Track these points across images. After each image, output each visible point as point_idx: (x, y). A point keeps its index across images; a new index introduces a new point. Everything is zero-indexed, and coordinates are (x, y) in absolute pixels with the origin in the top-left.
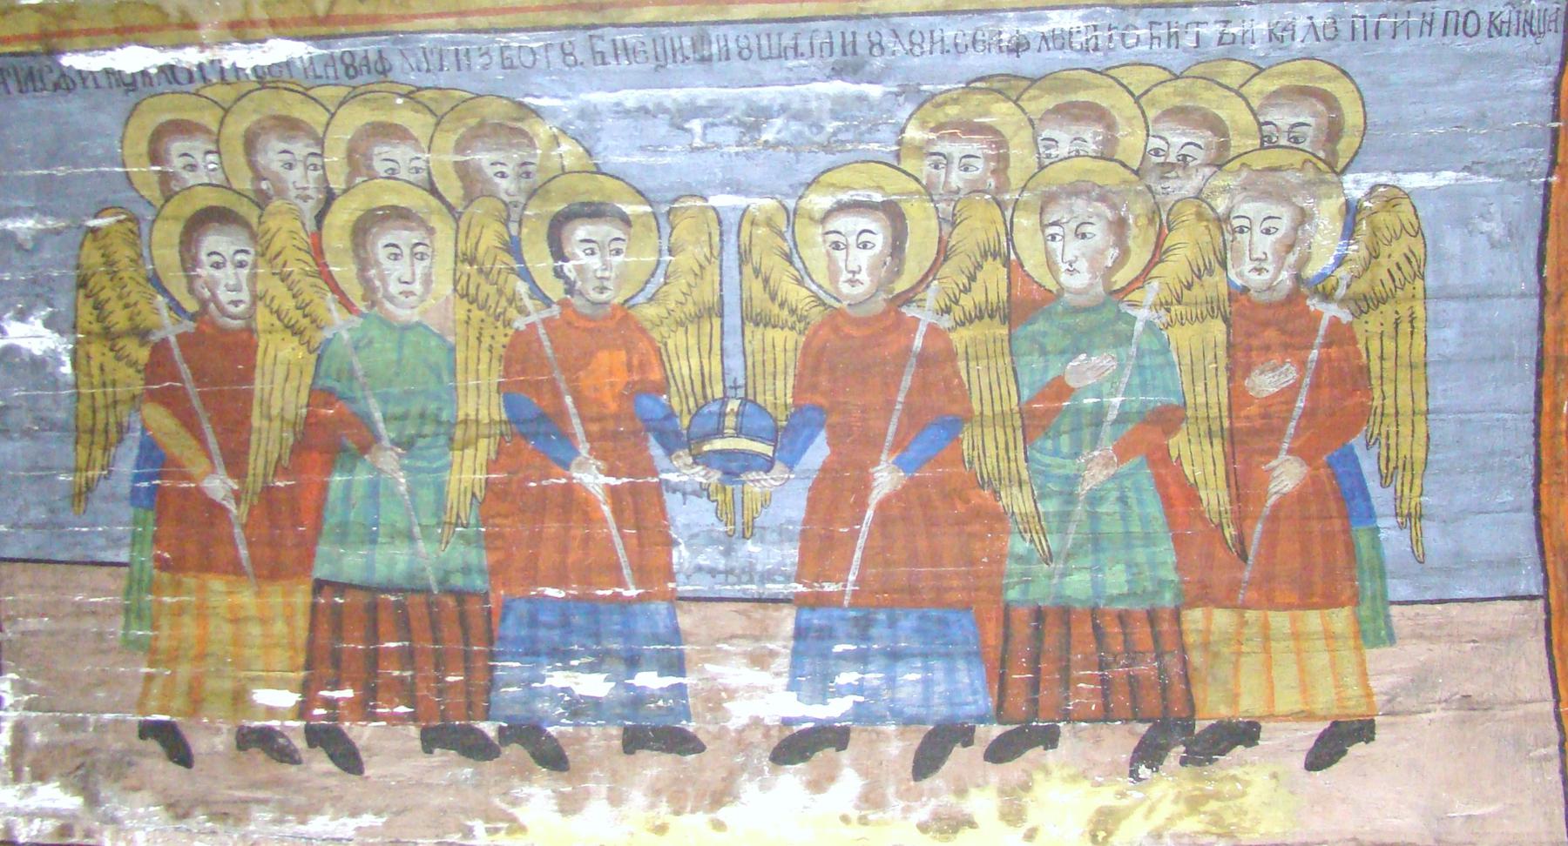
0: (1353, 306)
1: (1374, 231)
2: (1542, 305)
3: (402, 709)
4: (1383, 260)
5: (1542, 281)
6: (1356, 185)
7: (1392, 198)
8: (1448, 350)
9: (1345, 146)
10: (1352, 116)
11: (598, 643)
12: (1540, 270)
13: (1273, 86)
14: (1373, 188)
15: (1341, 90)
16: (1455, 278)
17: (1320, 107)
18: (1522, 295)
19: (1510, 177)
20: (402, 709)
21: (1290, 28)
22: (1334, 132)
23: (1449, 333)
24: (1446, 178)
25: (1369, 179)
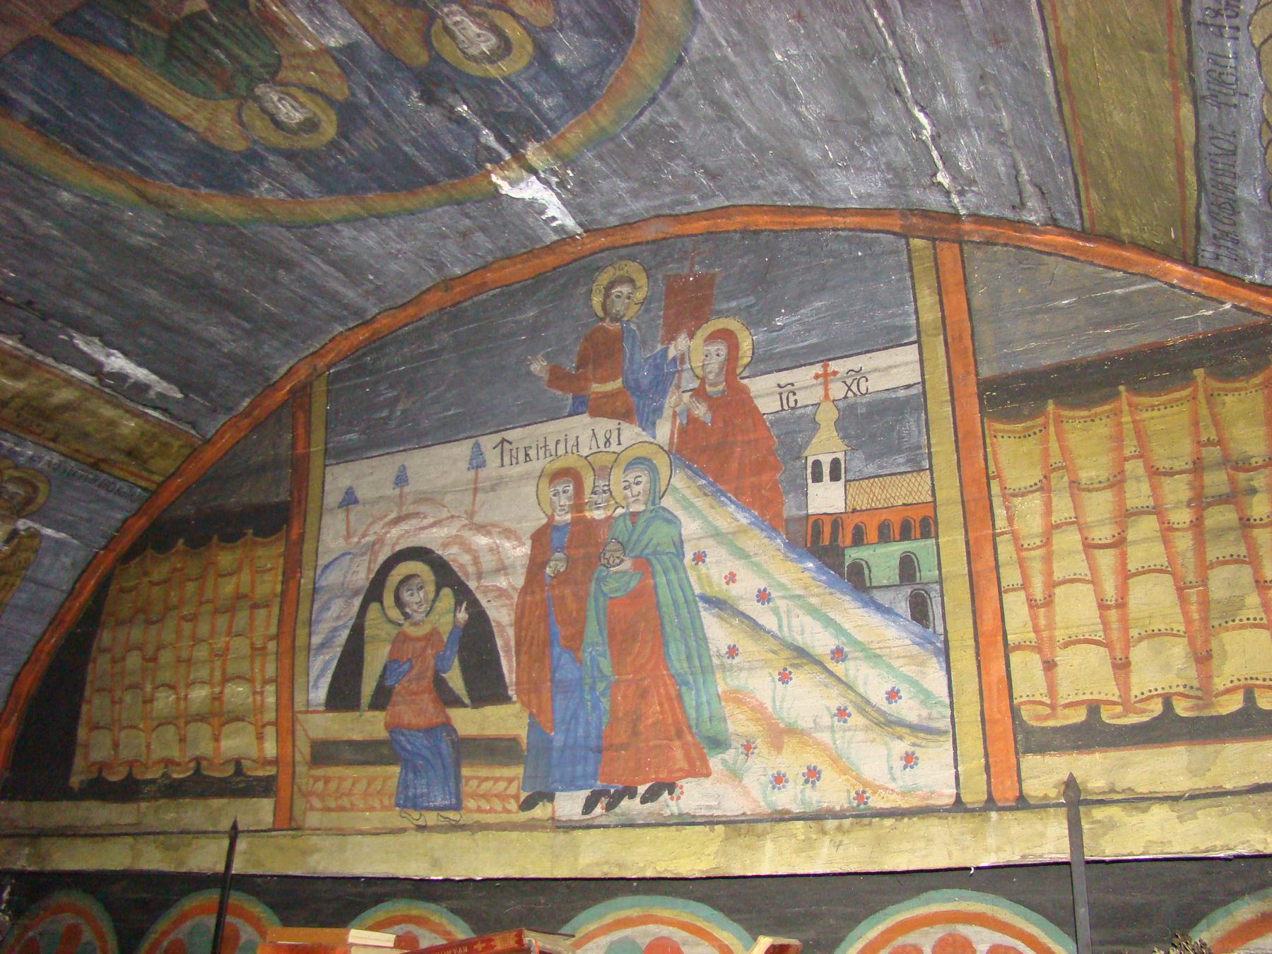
0: (744, 314)
1: (19, 543)
2: (68, 597)
3: (160, 221)
4: (15, 558)
5: (73, 588)
6: (22, 524)
7: (34, 535)
8: (20, 603)
9: (32, 508)
10: (41, 499)
11: (649, 185)
12: (75, 583)
13: (17, 474)
14: (29, 528)
15: (43, 488)
16: (40, 576)
17: (30, 490)
18: (62, 591)
19: (87, 545)
20: (160, 221)
21: (40, 458)
22: (29, 501)
23: (24, 596)
24: (62, 535)
25: (30, 523)
